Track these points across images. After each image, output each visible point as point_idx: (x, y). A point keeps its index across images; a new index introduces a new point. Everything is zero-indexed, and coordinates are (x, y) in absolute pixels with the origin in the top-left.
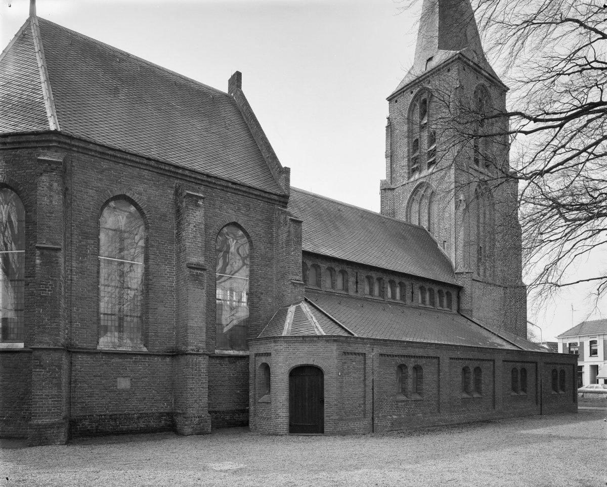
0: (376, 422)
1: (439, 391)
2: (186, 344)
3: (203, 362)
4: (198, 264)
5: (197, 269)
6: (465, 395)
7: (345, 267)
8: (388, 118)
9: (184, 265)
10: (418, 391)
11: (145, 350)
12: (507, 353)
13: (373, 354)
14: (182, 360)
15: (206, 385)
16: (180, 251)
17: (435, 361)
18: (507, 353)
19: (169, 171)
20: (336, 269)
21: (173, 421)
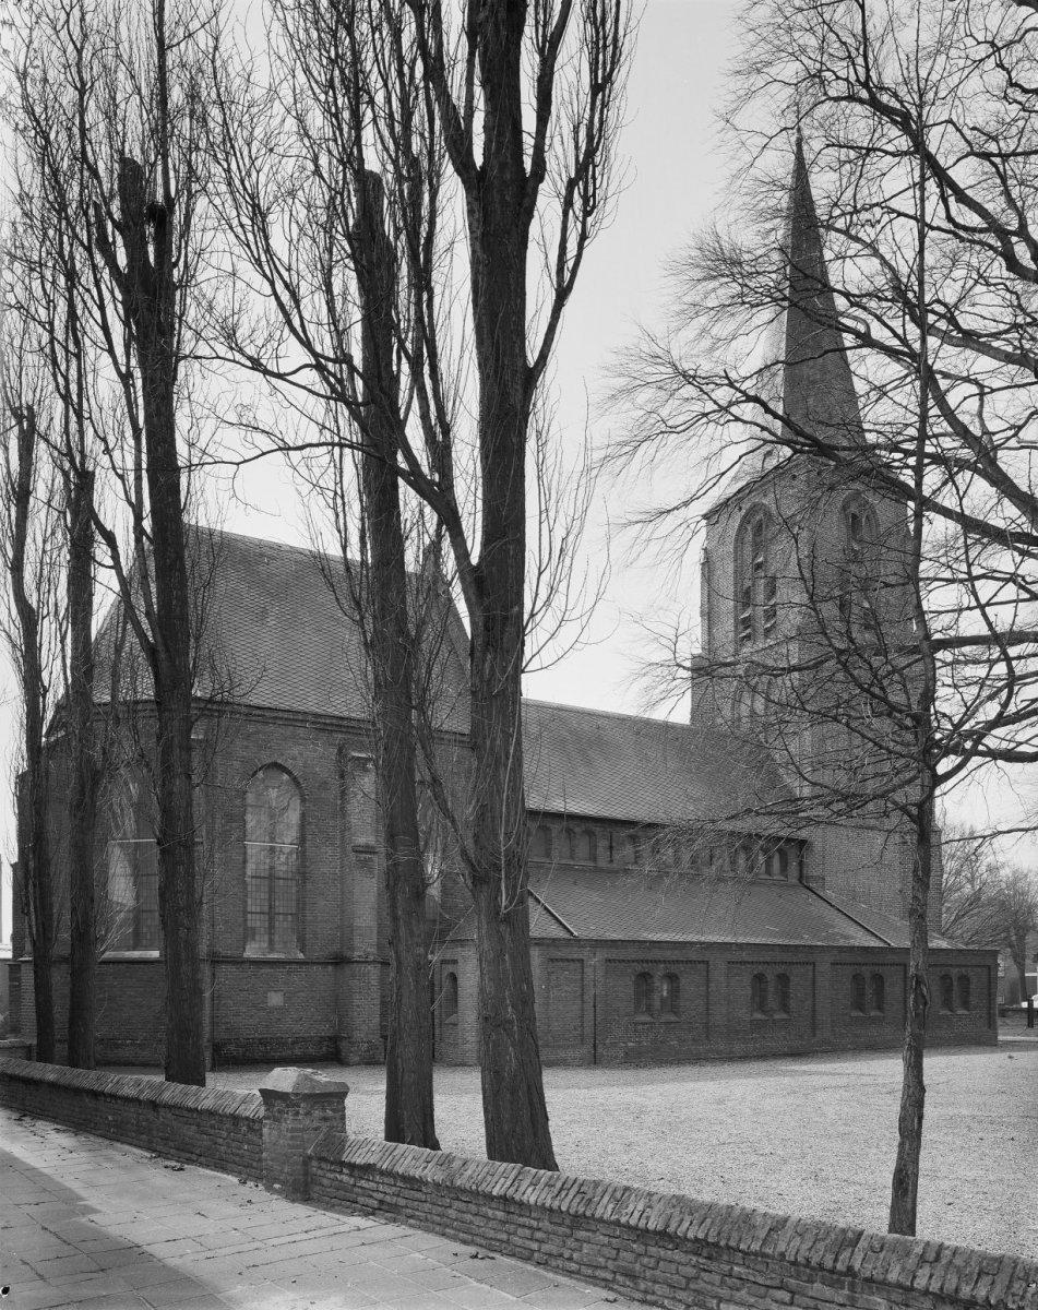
0: (600, 1050)
1: (708, 1009)
2: (352, 949)
3: (373, 972)
4: (367, 846)
5: (366, 852)
6: (758, 1016)
7: (591, 826)
8: (705, 550)
9: (349, 848)
10: (785, 1007)
11: (301, 956)
12: (840, 952)
13: (595, 960)
14: (347, 970)
15: (377, 1002)
16: (345, 829)
17: (701, 967)
18: (840, 952)
19: (332, 724)
20: (577, 830)
21: (337, 1048)
